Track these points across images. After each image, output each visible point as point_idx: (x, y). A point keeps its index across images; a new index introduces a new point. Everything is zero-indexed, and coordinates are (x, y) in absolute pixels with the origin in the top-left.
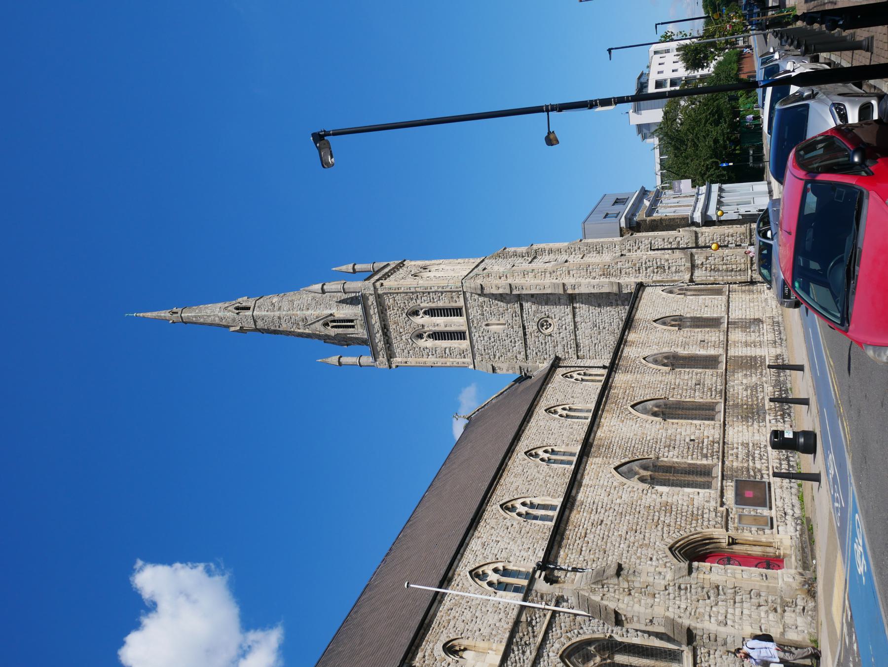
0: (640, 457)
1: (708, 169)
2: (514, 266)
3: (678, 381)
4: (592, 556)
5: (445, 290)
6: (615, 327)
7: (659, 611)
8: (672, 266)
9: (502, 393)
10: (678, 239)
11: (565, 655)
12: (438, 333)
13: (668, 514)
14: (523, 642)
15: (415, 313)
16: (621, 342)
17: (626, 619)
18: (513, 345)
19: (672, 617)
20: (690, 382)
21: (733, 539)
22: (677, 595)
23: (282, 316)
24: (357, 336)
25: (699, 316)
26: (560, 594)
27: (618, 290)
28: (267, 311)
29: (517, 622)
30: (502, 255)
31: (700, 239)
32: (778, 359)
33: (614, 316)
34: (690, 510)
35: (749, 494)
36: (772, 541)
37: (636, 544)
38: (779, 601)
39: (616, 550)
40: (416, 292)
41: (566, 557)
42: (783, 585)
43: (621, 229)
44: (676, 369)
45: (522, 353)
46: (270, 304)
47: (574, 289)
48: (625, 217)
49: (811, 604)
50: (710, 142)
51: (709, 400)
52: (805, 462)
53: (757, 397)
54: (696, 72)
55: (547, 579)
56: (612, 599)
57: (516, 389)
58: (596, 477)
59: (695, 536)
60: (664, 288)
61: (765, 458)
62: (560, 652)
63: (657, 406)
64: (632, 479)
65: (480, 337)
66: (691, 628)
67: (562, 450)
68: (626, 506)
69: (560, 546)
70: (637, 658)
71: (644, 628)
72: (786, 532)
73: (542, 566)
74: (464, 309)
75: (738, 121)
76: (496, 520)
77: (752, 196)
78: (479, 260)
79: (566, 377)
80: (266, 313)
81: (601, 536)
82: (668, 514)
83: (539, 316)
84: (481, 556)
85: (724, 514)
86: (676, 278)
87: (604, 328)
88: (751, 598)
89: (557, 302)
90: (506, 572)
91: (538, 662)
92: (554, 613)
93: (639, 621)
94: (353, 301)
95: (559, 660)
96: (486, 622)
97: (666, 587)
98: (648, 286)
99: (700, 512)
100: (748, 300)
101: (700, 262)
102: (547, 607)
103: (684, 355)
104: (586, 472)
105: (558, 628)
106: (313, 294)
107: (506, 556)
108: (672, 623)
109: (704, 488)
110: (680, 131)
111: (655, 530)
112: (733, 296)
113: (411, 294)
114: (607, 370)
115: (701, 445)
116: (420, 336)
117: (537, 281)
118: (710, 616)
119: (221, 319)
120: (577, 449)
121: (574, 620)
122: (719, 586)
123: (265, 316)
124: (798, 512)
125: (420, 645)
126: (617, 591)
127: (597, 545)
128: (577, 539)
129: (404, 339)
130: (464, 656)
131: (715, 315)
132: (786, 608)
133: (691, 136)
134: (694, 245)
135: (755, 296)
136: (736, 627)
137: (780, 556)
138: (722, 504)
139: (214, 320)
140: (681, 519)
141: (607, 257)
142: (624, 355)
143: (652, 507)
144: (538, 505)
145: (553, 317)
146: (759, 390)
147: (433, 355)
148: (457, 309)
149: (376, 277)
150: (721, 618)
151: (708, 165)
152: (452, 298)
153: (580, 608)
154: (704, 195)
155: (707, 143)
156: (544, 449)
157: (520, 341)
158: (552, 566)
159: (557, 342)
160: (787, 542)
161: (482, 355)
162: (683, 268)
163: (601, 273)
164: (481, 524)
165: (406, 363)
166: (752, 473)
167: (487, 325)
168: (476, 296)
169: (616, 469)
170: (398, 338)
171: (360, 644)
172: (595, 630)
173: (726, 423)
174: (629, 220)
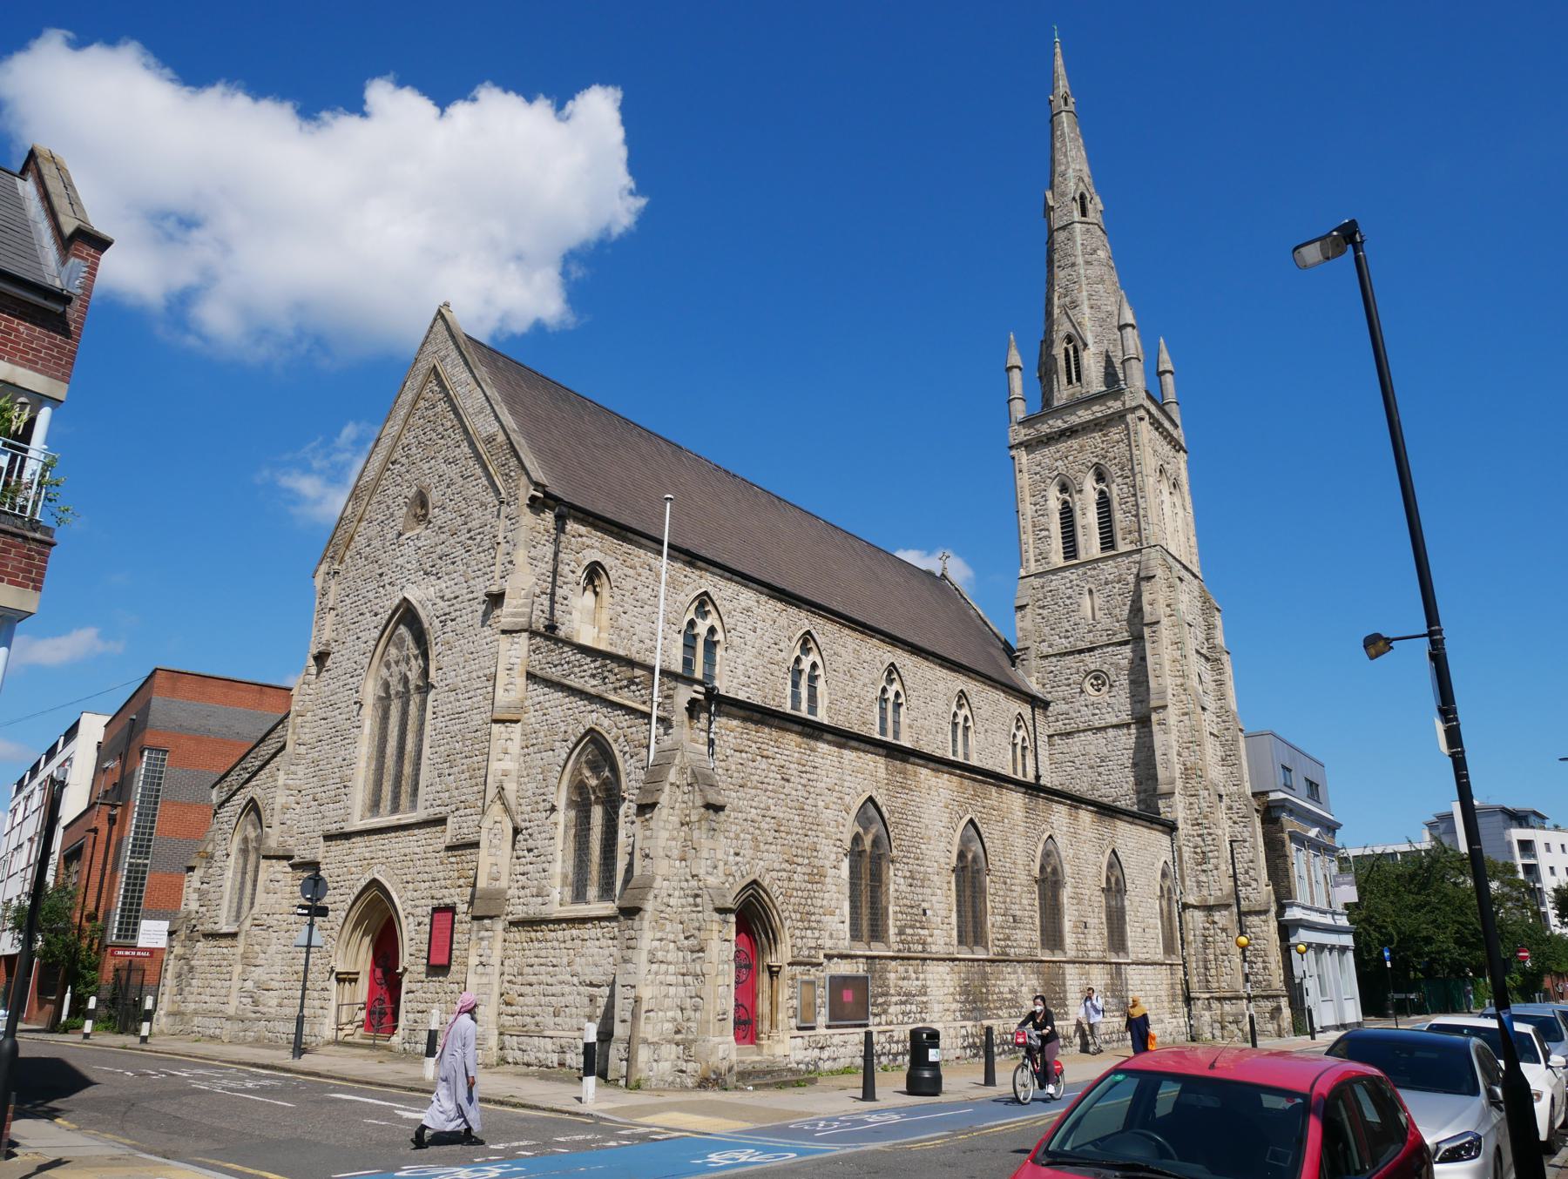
0: (892, 835)
1: (1379, 928)
2: (1191, 626)
3: (1018, 888)
4: (733, 767)
5: (1142, 519)
6: (1103, 791)
7: (662, 867)
8: (1207, 876)
9: (985, 623)
10: (1254, 884)
11: (595, 734)
12: (1072, 516)
13: (806, 878)
14: (606, 674)
15: (1100, 477)
16: (1076, 801)
17: (647, 820)
18: (1062, 635)
19: (655, 885)
20: (1017, 907)
21: (778, 972)
22: (686, 892)
23: (1076, 268)
24: (1055, 390)
25: (1128, 920)
26: (674, 723)
27: (1163, 792)
28: (1082, 244)
29: (630, 663)
30: (1208, 607)
31: (1256, 918)
32: (1064, 1039)
33: (1120, 787)
34: (817, 910)
35: (848, 996)
36: (780, 1029)
37: (757, 832)
38: (691, 1037)
39: (745, 803)
40: (1134, 475)
41: (728, 729)
42: (712, 1043)
43: (1265, 793)
44: (1036, 887)
45: (1050, 650)
46: (1094, 246)
47: (1159, 724)
48: (1285, 800)
49: (690, 1082)
50: (1426, 930)
51: (991, 936)
52: (891, 1085)
53: (1000, 1008)
54: (1552, 905)
55: (693, 702)
56: (674, 798)
57: (993, 645)
58: (855, 769)
59: (777, 918)
60: (1170, 864)
61: (906, 1019)
62: (598, 728)
63: (975, 859)
64: (856, 823)
65: (1071, 581)
66: (642, 913)
67: (902, 719)
68: (815, 815)
69: (744, 720)
70: (599, 837)
71: (637, 846)
72: (794, 1049)
73: (712, 696)
74: (1113, 553)
75: (1467, 975)
76: (786, 625)
77: (1335, 999)
78: (1196, 570)
79: (1018, 720)
80: (1079, 242)
81: (766, 780)
82: (806, 878)
83: (1112, 672)
84: (731, 607)
85: (814, 960)
86: (1188, 883)
87: (1100, 774)
88: (691, 997)
89: (1135, 698)
90: (711, 645)
91: (583, 697)
92: (647, 716)
93: (646, 838)
94: (1110, 376)
95: (587, 727)
96: (638, 620)
97: (697, 876)
98: (1172, 840)
99: (814, 925)
100: (1158, 993)
101: (1216, 918)
102: (655, 705)
103: (1061, 898)
104: (862, 754)
105: (629, 723)
106: (1116, 312)
107: (734, 643)
108: (647, 886)
109: (851, 930)
110: (1443, 882)
111: (781, 860)
112: (1165, 970)
113: (1130, 467)
114: (1033, 781)
115: (918, 924)
116: (1064, 488)
117: (1167, 665)
118: (661, 940)
119: (1063, 175)
120: (905, 742)
121: (641, 745)
122: (703, 952)
123: (1075, 242)
124: (827, 1065)
125: (596, 528)
126: (685, 805)
127: (751, 774)
128: (758, 745)
129: (1057, 464)
130: (587, 592)
131: (1130, 944)
132: (682, 1047)
133: (1434, 900)
134: (1244, 909)
135: (1166, 1004)
136: (649, 977)
137: (759, 1039)
138: (829, 957)
139: (1060, 165)
140: (802, 897)
141: (1215, 773)
142: (1055, 806)
143: (815, 854)
144: (815, 688)
145: (1112, 694)
146: (1012, 1011)
147: (1036, 511)
148: (1112, 541)
149: (1153, 409)
150: (660, 955)
151: (1386, 928)
152: (1130, 532)
153: (658, 752)
154: (1333, 923)
155: (1424, 926)
156: (902, 692)
157: (1068, 645)
158: (713, 708)
159: (1072, 702)
160: (779, 1050)
161: (1043, 587)
162: (1205, 892)
163: (1189, 765)
164: (779, 605)
165: (1020, 471)
166: (880, 1000)
167: (1090, 591)
168: (1135, 571)
169: (871, 799)
170: (1058, 455)
171: (595, 445)
172: (631, 777)
173: (957, 963)
174: (1282, 805)
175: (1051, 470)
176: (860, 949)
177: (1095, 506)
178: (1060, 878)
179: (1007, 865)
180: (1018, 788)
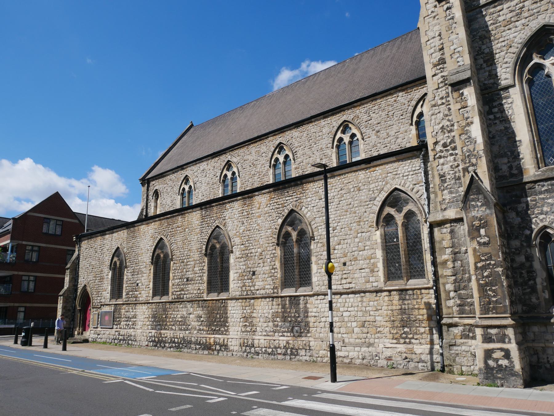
51: (171, 290)
166: (118, 320)
176: (114, 302)
180: (194, 210)
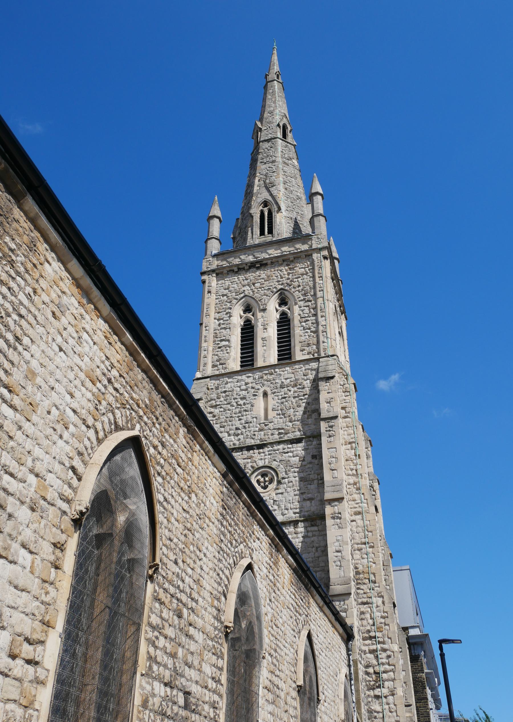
3: (199, 637)
8: (381, 704)
15: (283, 302)
20: (192, 674)
23: (276, 163)
47: (333, 518)
65: (246, 384)
80: (280, 149)
89: (304, 496)
113: (312, 293)
119: (271, 113)
129: (245, 288)
145: (280, 491)
147: (219, 325)
152: (309, 345)
161: (217, 388)
163: (361, 568)
165: (209, 292)
167: (265, 394)
168: (311, 377)
170: (246, 282)
175: (237, 293)
177: (276, 324)
178: (257, 647)
179: (187, 579)
